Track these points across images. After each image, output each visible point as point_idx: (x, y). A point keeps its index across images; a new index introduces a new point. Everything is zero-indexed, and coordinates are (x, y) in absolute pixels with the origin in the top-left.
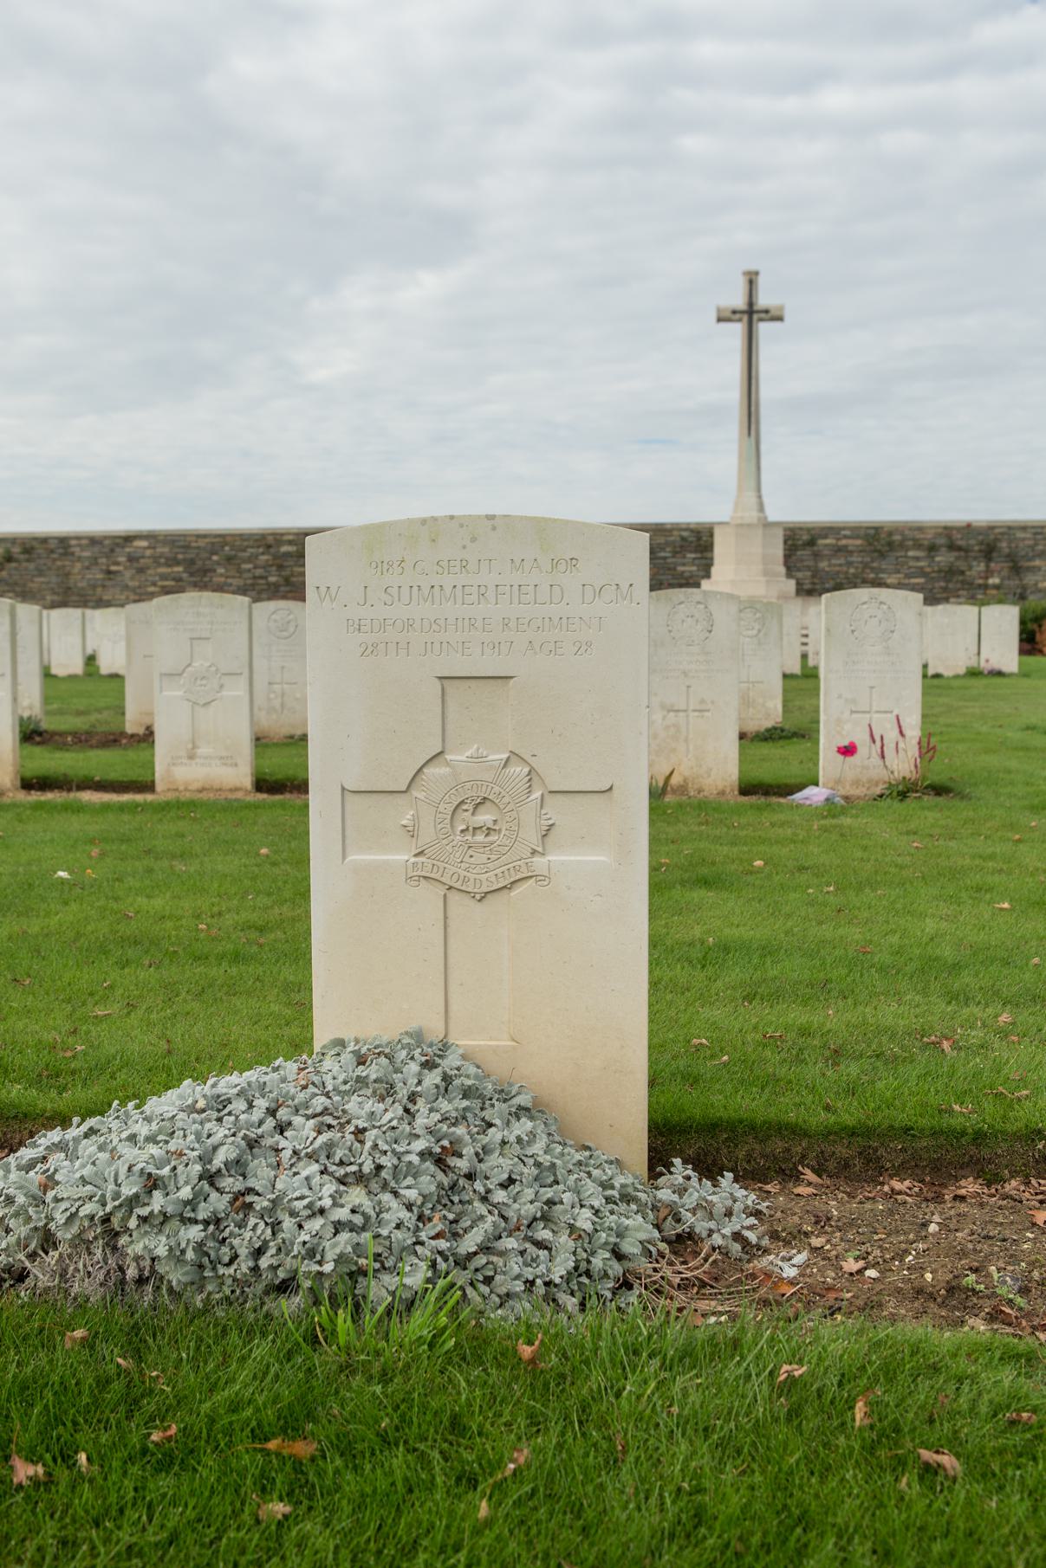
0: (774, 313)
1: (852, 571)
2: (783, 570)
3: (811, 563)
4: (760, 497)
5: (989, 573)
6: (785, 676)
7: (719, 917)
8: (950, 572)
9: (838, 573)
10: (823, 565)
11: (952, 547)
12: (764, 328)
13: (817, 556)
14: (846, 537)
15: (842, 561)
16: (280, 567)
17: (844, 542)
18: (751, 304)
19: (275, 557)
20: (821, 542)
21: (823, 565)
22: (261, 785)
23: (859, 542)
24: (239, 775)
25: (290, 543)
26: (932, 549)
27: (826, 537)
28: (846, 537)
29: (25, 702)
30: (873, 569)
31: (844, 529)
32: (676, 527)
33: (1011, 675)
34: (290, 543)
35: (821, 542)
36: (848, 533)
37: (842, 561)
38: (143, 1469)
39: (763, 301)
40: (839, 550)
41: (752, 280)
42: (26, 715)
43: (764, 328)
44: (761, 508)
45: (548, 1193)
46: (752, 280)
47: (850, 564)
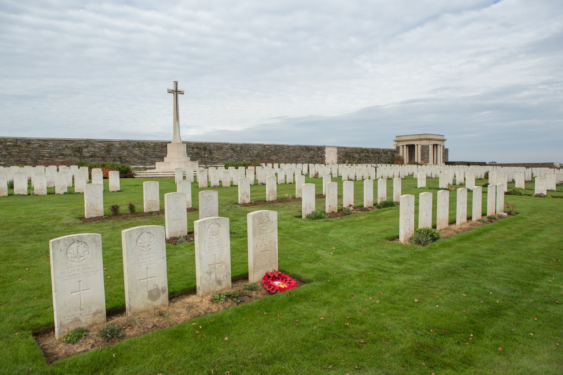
5: (205, 154)
6: (547, 191)
8: (197, 154)
11: (197, 148)
12: (180, 96)
16: (7, 149)
18: (176, 89)
19: (5, 146)
22: (48, 194)
24: (45, 192)
25: (10, 142)
26: (193, 148)
29: (379, 195)
32: (133, 141)
34: (10, 142)
38: (22, 296)
39: (179, 89)
41: (176, 83)
43: (180, 96)
46: (176, 83)
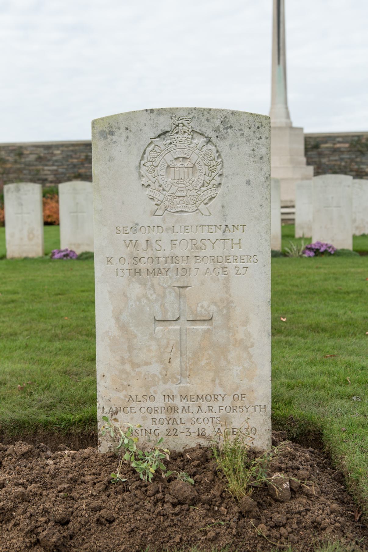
0: (163, 137)
1: (343, 164)
2: (304, 160)
3: (317, 160)
4: (287, 108)
7: (93, 378)
9: (335, 165)
10: (324, 160)
13: (320, 155)
14: (339, 142)
15: (337, 158)
17: (338, 145)
20: (323, 146)
21: (324, 160)
23: (347, 145)
27: (326, 142)
28: (339, 142)
30: (357, 163)
31: (338, 137)
33: (338, 254)
35: (323, 146)
36: (340, 139)
37: (337, 158)
40: (335, 151)
42: (325, 432)
44: (288, 116)
45: (218, 530)
47: (342, 159)
